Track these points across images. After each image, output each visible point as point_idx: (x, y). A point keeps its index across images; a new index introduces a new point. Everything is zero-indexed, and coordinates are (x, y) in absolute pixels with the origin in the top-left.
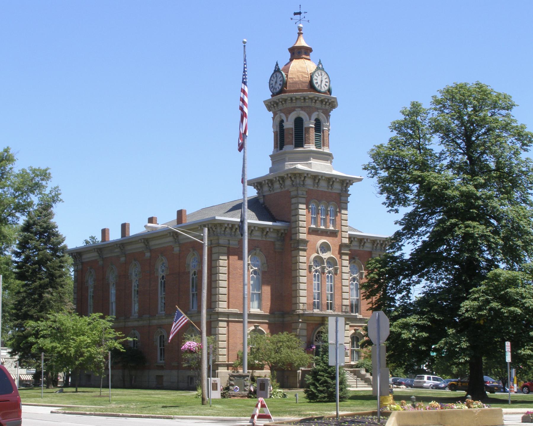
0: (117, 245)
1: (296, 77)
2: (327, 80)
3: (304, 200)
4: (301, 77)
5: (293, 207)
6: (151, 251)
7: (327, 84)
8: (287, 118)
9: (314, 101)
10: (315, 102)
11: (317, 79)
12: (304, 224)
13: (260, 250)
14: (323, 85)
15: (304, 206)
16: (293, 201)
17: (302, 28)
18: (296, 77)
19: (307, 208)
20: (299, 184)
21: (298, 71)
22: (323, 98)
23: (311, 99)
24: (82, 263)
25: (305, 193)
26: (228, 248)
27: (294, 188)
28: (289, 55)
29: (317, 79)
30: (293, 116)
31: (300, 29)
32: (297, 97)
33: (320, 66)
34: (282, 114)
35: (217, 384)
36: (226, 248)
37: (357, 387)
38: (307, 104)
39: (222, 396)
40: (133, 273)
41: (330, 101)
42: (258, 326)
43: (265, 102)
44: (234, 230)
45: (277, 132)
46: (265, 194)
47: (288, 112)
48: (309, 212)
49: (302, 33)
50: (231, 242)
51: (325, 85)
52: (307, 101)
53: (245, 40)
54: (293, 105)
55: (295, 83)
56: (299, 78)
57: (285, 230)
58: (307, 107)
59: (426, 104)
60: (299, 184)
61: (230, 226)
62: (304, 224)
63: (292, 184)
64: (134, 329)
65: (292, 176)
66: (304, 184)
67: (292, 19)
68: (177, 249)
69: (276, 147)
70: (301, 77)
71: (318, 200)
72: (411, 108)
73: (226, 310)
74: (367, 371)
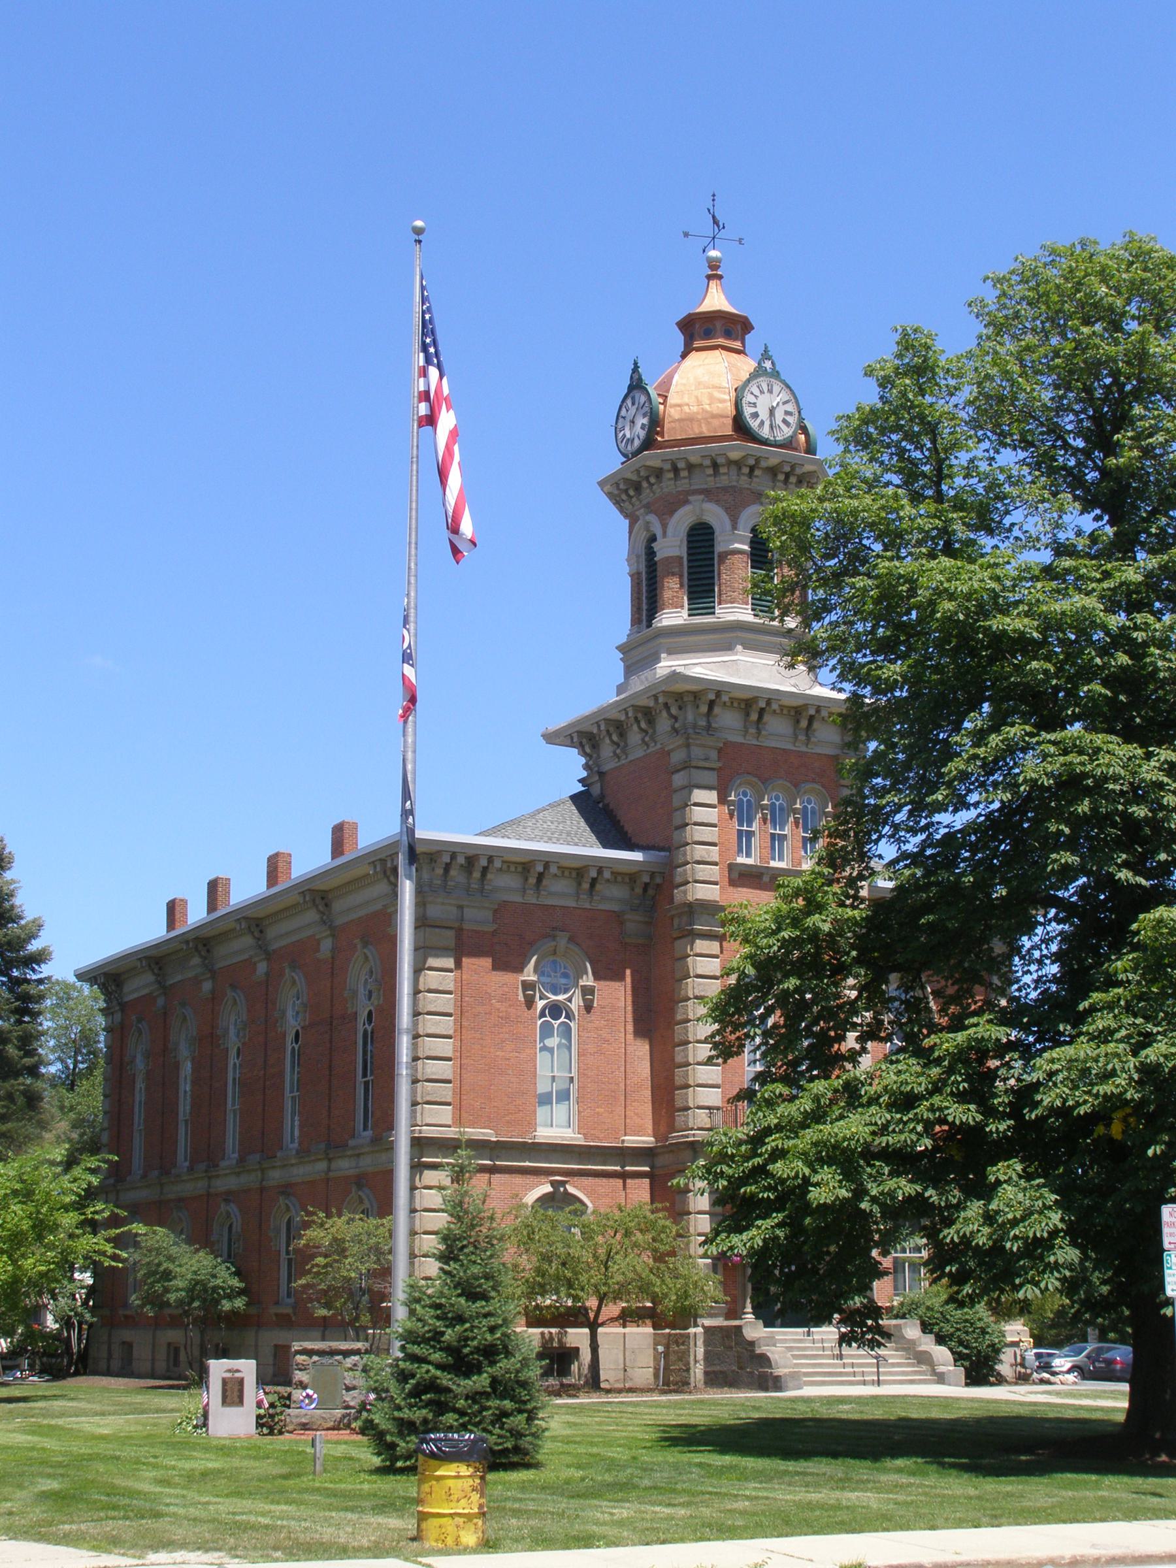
0: (187, 942)
1: (692, 401)
2: (790, 407)
3: (712, 777)
4: (706, 401)
5: (676, 800)
6: (269, 956)
7: (789, 419)
8: (664, 526)
9: (746, 470)
10: (751, 474)
11: (755, 405)
12: (714, 853)
13: (571, 939)
14: (779, 415)
15: (711, 797)
16: (678, 779)
17: (719, 260)
18: (692, 401)
19: (722, 800)
20: (695, 726)
21: (699, 384)
22: (773, 461)
23: (738, 464)
24: (123, 1007)
25: (714, 755)
26: (459, 931)
27: (679, 741)
28: (680, 338)
29: (755, 405)
30: (682, 520)
31: (714, 265)
32: (694, 459)
33: (768, 365)
34: (652, 518)
35: (241, 1382)
36: (451, 934)
37: (879, 1383)
38: (723, 481)
39: (259, 1425)
40: (232, 1027)
41: (798, 471)
42: (563, 1183)
43: (602, 484)
44: (477, 875)
45: (639, 573)
46: (606, 767)
47: (667, 508)
48: (731, 816)
49: (720, 277)
50: (469, 913)
51: (784, 421)
52: (723, 470)
53: (419, 223)
54: (683, 484)
55: (690, 419)
56: (699, 403)
57: (653, 875)
58: (725, 489)
59: (956, 338)
60: (695, 726)
61: (461, 860)
62: (714, 853)
63: (673, 728)
64: (227, 1201)
65: (670, 701)
66: (709, 727)
67: (686, 235)
68: (326, 945)
69: (636, 621)
70: (706, 401)
71: (760, 778)
72: (900, 356)
73: (451, 1133)
74: (926, 1327)
